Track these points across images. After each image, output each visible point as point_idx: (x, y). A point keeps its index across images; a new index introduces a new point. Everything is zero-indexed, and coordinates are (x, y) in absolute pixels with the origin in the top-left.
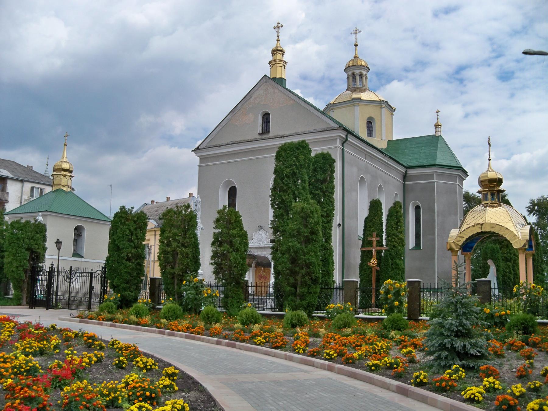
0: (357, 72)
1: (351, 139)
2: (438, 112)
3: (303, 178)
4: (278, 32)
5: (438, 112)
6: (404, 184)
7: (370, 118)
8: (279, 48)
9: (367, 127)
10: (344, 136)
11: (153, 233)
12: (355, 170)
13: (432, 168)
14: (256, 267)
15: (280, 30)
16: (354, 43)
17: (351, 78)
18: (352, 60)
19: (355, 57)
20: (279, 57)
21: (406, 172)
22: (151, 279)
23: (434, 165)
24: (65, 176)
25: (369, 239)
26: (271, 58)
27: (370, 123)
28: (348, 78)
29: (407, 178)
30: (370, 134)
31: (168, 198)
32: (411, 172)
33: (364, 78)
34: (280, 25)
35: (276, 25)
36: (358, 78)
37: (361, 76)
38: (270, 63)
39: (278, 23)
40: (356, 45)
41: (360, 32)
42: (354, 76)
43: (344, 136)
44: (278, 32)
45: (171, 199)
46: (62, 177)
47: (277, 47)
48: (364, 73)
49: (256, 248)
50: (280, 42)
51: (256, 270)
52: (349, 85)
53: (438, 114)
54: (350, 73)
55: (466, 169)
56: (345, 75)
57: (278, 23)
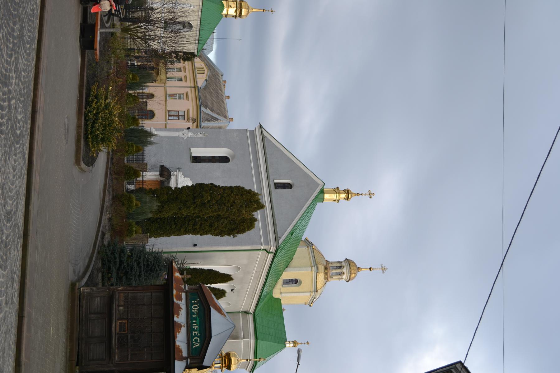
0: (344, 270)
1: (270, 256)
2: (308, 343)
3: (226, 210)
4: (366, 194)
5: (308, 343)
6: (239, 312)
7: (301, 283)
8: (350, 195)
9: (292, 280)
10: (271, 251)
11: (193, 85)
12: (245, 262)
13: (254, 337)
14: (161, 181)
15: (368, 196)
16: (372, 267)
17: (339, 265)
18: (355, 265)
19: (359, 269)
20: (344, 196)
21: (251, 313)
22: (146, 102)
23: (256, 338)
24: (236, 11)
25: (185, 272)
26: (342, 188)
27: (295, 282)
28: (339, 262)
29: (245, 314)
30: (287, 282)
31: (228, 97)
32: (251, 318)
33: (339, 277)
34: (372, 195)
35: (372, 192)
36: (339, 271)
37: (341, 274)
38: (337, 188)
39: (373, 194)
40: (370, 269)
41: (383, 273)
42: (341, 267)
43: (271, 251)
44: (366, 194)
45: (227, 100)
46: (235, 9)
47: (352, 193)
48: (344, 277)
49: (177, 180)
50: (357, 196)
51: (157, 181)
52: (332, 263)
53: (306, 344)
54: (343, 264)
55: (255, 371)
56: (342, 259)
57: (373, 194)
